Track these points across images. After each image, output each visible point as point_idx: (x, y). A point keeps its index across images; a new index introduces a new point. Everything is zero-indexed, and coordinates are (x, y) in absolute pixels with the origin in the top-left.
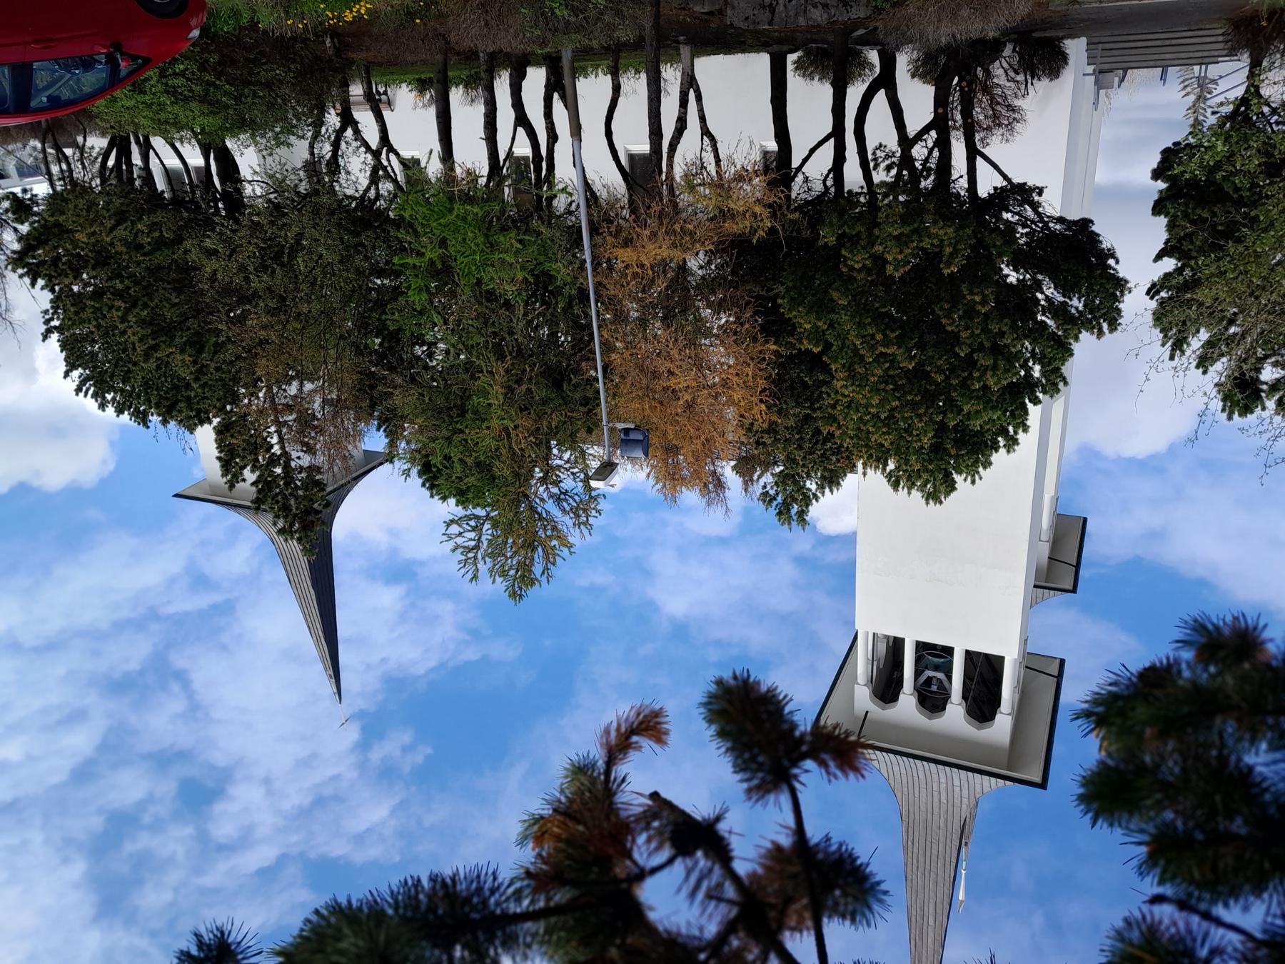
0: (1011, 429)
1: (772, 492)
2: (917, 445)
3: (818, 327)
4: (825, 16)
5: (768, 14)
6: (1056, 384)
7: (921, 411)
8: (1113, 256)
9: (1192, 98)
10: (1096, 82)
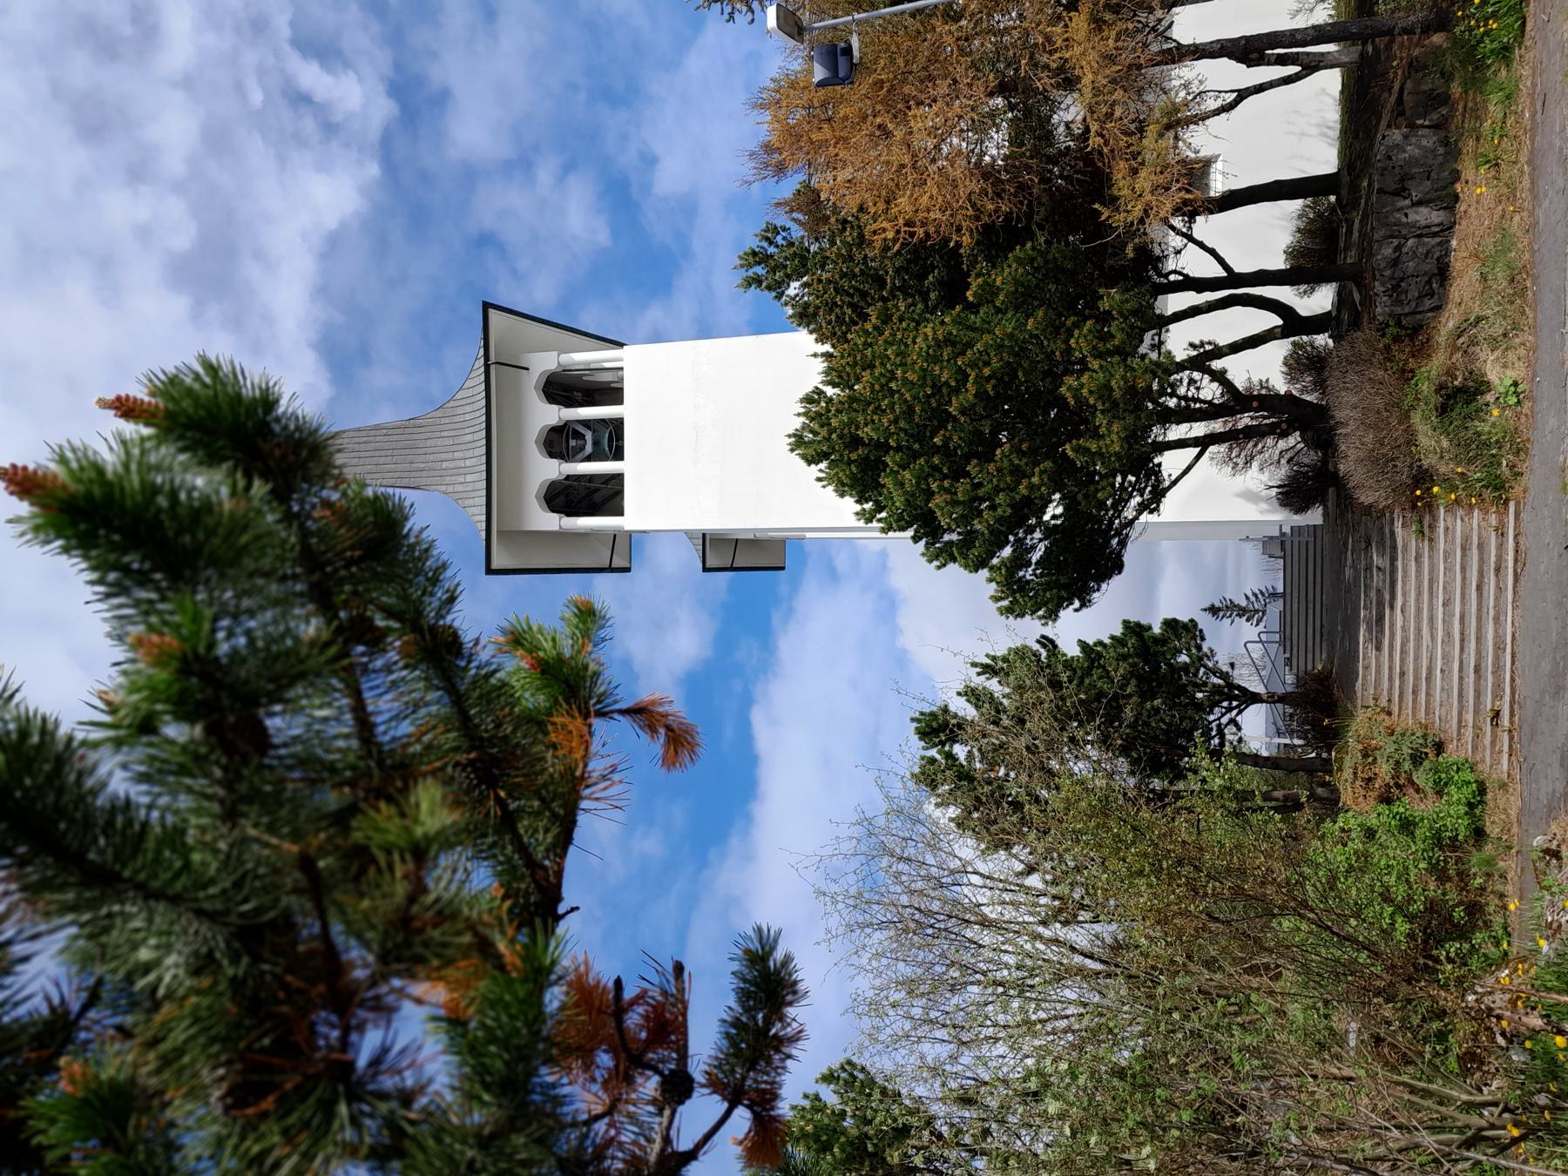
0: (883, 515)
1: (779, 239)
2: (861, 419)
3: (997, 295)
4: (1383, 265)
5: (1393, 187)
6: (937, 558)
7: (902, 424)
8: (1083, 605)
9: (1243, 603)
10: (1271, 538)
